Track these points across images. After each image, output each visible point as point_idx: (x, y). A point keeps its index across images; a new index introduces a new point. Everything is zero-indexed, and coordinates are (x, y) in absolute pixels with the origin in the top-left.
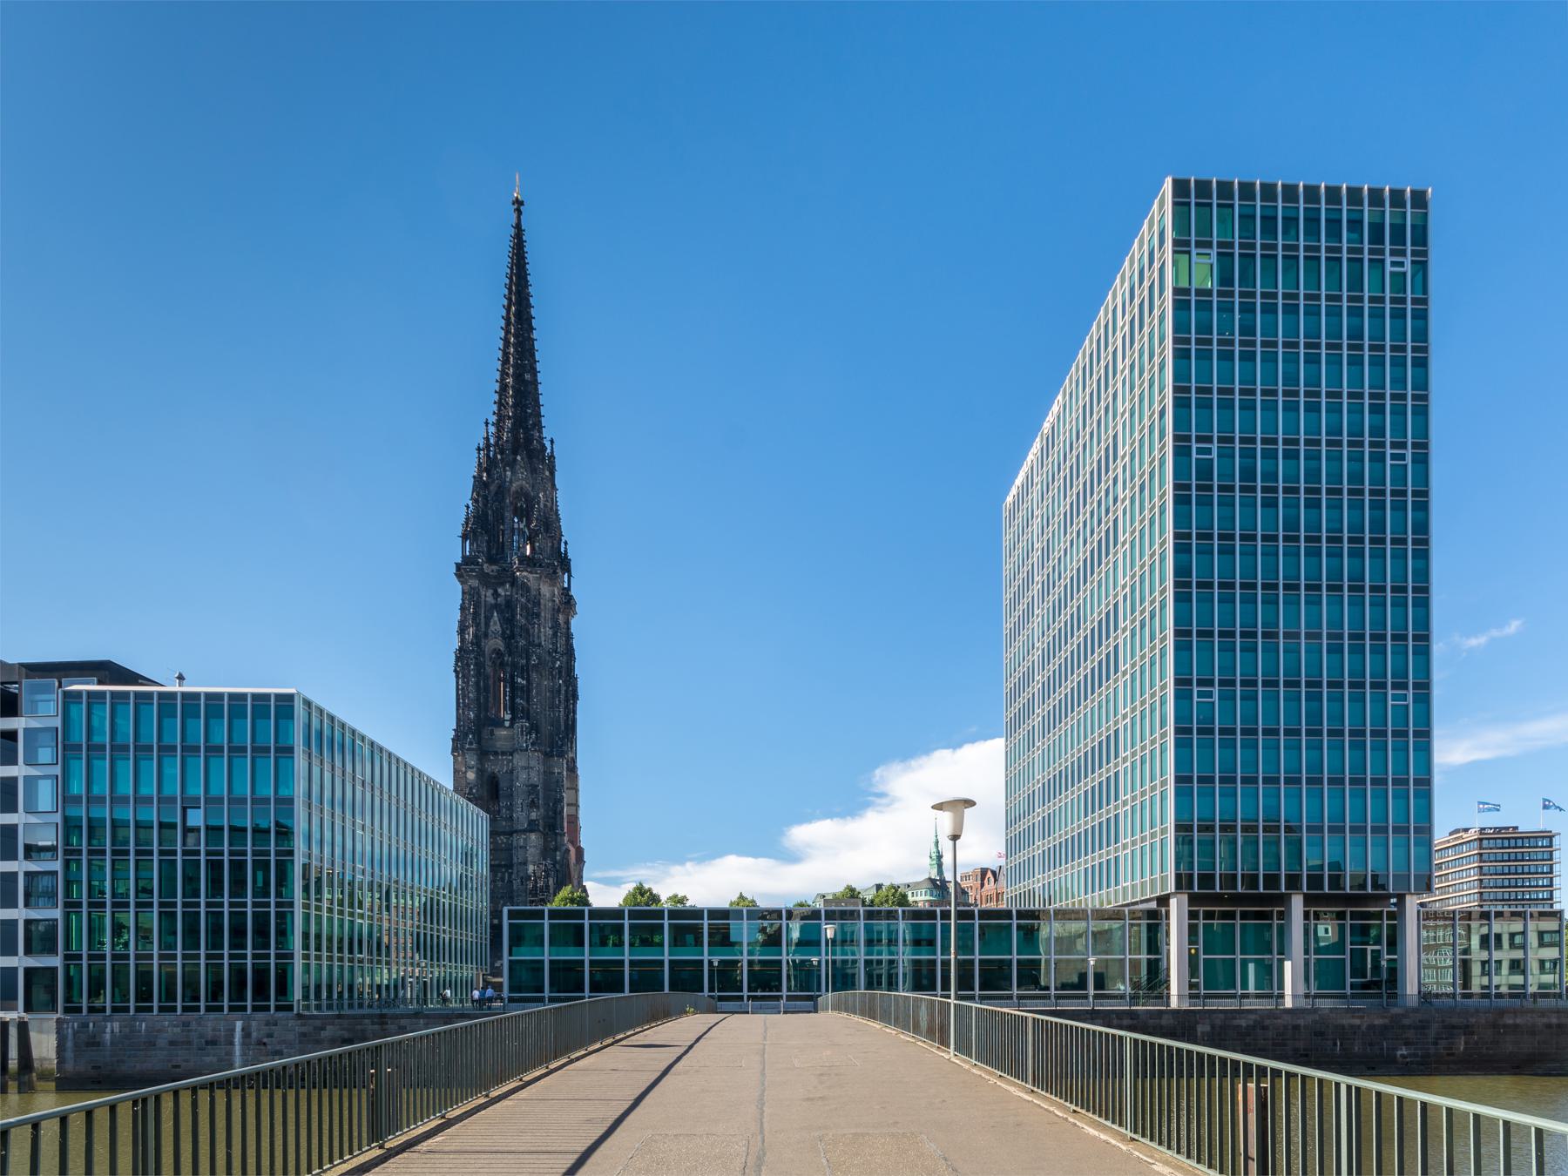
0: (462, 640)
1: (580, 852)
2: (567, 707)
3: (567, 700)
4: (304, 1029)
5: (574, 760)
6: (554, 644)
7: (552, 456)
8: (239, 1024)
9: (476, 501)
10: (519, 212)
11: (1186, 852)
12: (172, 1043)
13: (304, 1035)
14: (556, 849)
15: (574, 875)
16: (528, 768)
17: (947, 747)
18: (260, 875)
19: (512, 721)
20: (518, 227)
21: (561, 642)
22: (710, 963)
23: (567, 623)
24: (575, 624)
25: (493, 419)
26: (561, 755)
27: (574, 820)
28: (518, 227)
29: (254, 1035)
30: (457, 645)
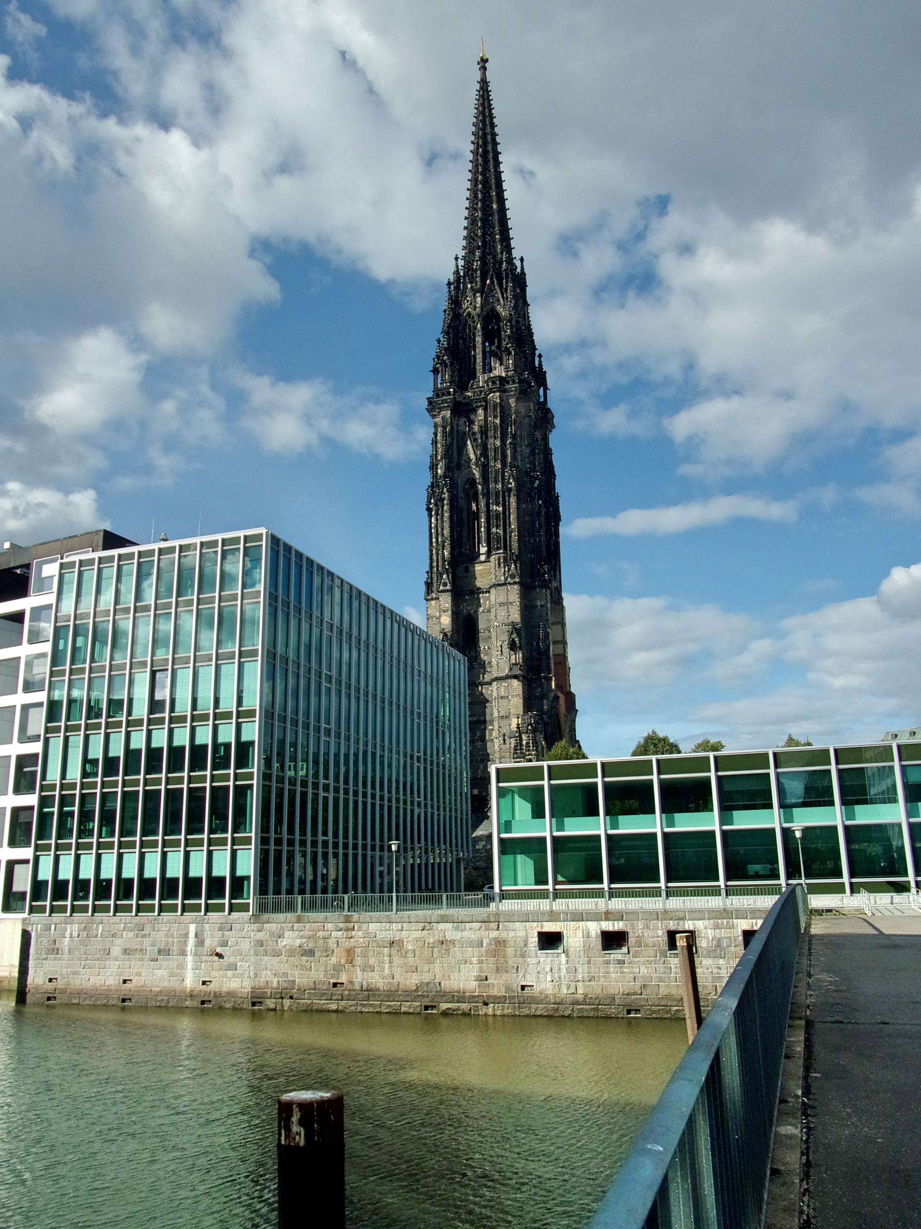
0: (435, 476)
1: (571, 699)
2: (548, 531)
3: (548, 523)
4: (260, 936)
5: (559, 591)
6: (532, 463)
7: (523, 273)
8: (192, 928)
9: (446, 333)
10: (484, 69)
11: (127, 821)
12: (126, 951)
13: (261, 943)
14: (543, 697)
15: (565, 727)
16: (507, 604)
17: (884, 578)
18: (61, 647)
19: (489, 554)
20: (484, 85)
21: (539, 459)
22: (787, 833)
23: (545, 439)
24: (555, 440)
25: (461, 253)
26: (545, 585)
27: (562, 660)
28: (484, 85)
29: (208, 942)
30: (428, 480)
